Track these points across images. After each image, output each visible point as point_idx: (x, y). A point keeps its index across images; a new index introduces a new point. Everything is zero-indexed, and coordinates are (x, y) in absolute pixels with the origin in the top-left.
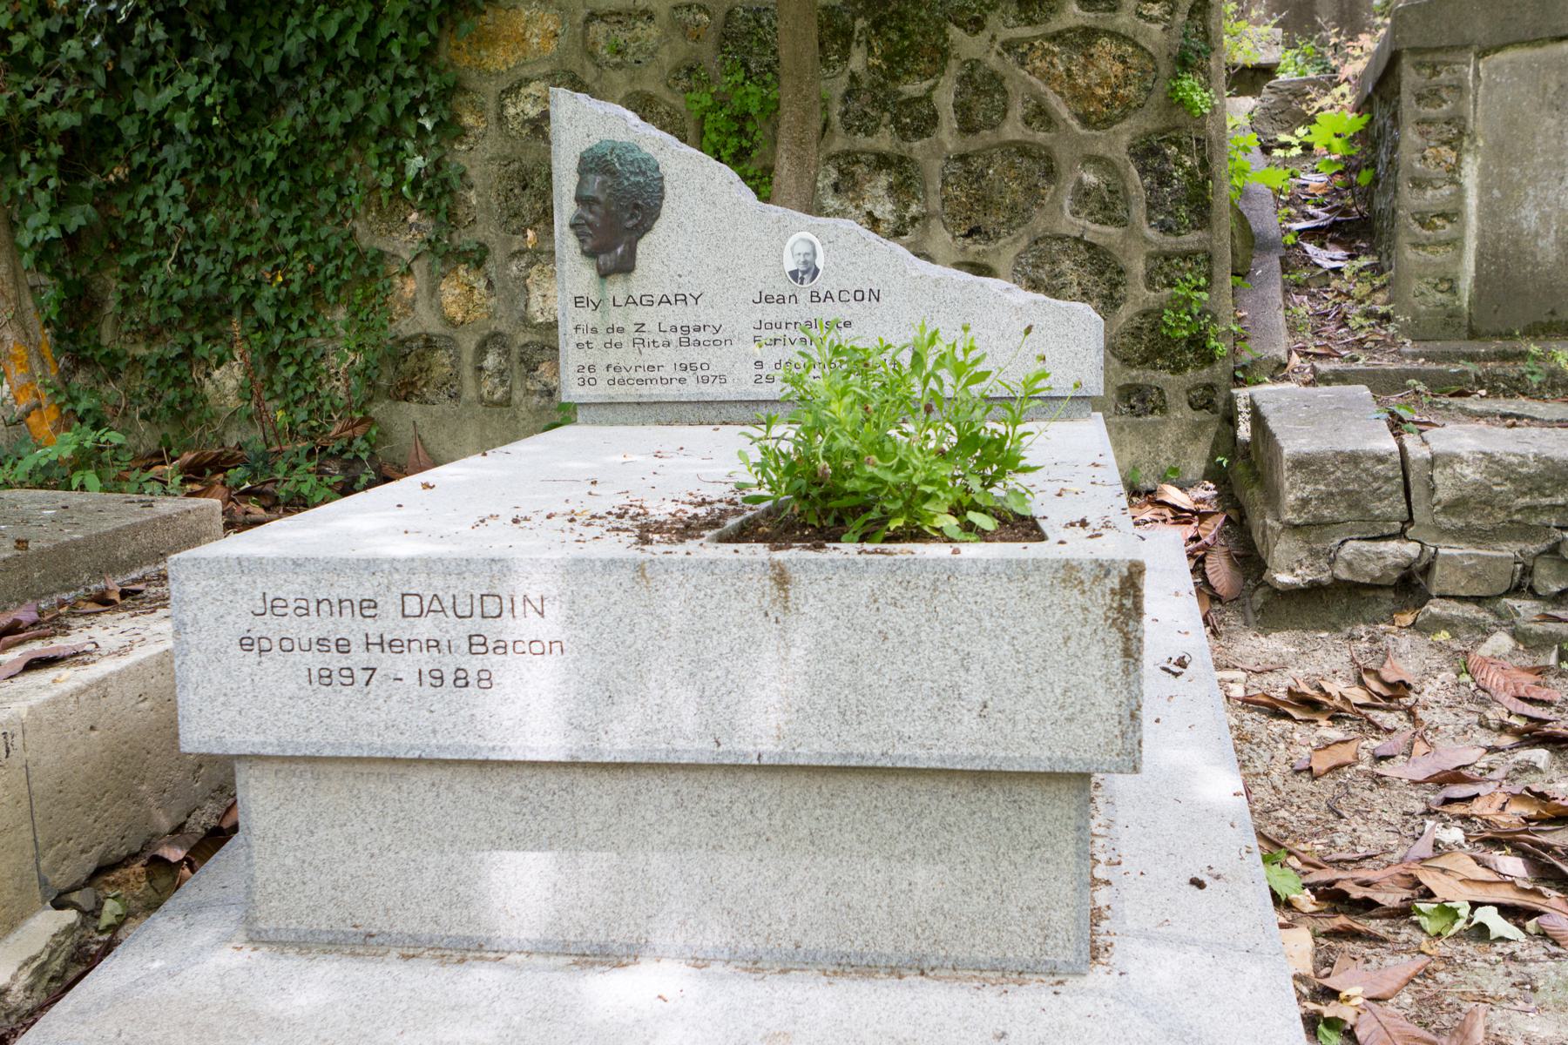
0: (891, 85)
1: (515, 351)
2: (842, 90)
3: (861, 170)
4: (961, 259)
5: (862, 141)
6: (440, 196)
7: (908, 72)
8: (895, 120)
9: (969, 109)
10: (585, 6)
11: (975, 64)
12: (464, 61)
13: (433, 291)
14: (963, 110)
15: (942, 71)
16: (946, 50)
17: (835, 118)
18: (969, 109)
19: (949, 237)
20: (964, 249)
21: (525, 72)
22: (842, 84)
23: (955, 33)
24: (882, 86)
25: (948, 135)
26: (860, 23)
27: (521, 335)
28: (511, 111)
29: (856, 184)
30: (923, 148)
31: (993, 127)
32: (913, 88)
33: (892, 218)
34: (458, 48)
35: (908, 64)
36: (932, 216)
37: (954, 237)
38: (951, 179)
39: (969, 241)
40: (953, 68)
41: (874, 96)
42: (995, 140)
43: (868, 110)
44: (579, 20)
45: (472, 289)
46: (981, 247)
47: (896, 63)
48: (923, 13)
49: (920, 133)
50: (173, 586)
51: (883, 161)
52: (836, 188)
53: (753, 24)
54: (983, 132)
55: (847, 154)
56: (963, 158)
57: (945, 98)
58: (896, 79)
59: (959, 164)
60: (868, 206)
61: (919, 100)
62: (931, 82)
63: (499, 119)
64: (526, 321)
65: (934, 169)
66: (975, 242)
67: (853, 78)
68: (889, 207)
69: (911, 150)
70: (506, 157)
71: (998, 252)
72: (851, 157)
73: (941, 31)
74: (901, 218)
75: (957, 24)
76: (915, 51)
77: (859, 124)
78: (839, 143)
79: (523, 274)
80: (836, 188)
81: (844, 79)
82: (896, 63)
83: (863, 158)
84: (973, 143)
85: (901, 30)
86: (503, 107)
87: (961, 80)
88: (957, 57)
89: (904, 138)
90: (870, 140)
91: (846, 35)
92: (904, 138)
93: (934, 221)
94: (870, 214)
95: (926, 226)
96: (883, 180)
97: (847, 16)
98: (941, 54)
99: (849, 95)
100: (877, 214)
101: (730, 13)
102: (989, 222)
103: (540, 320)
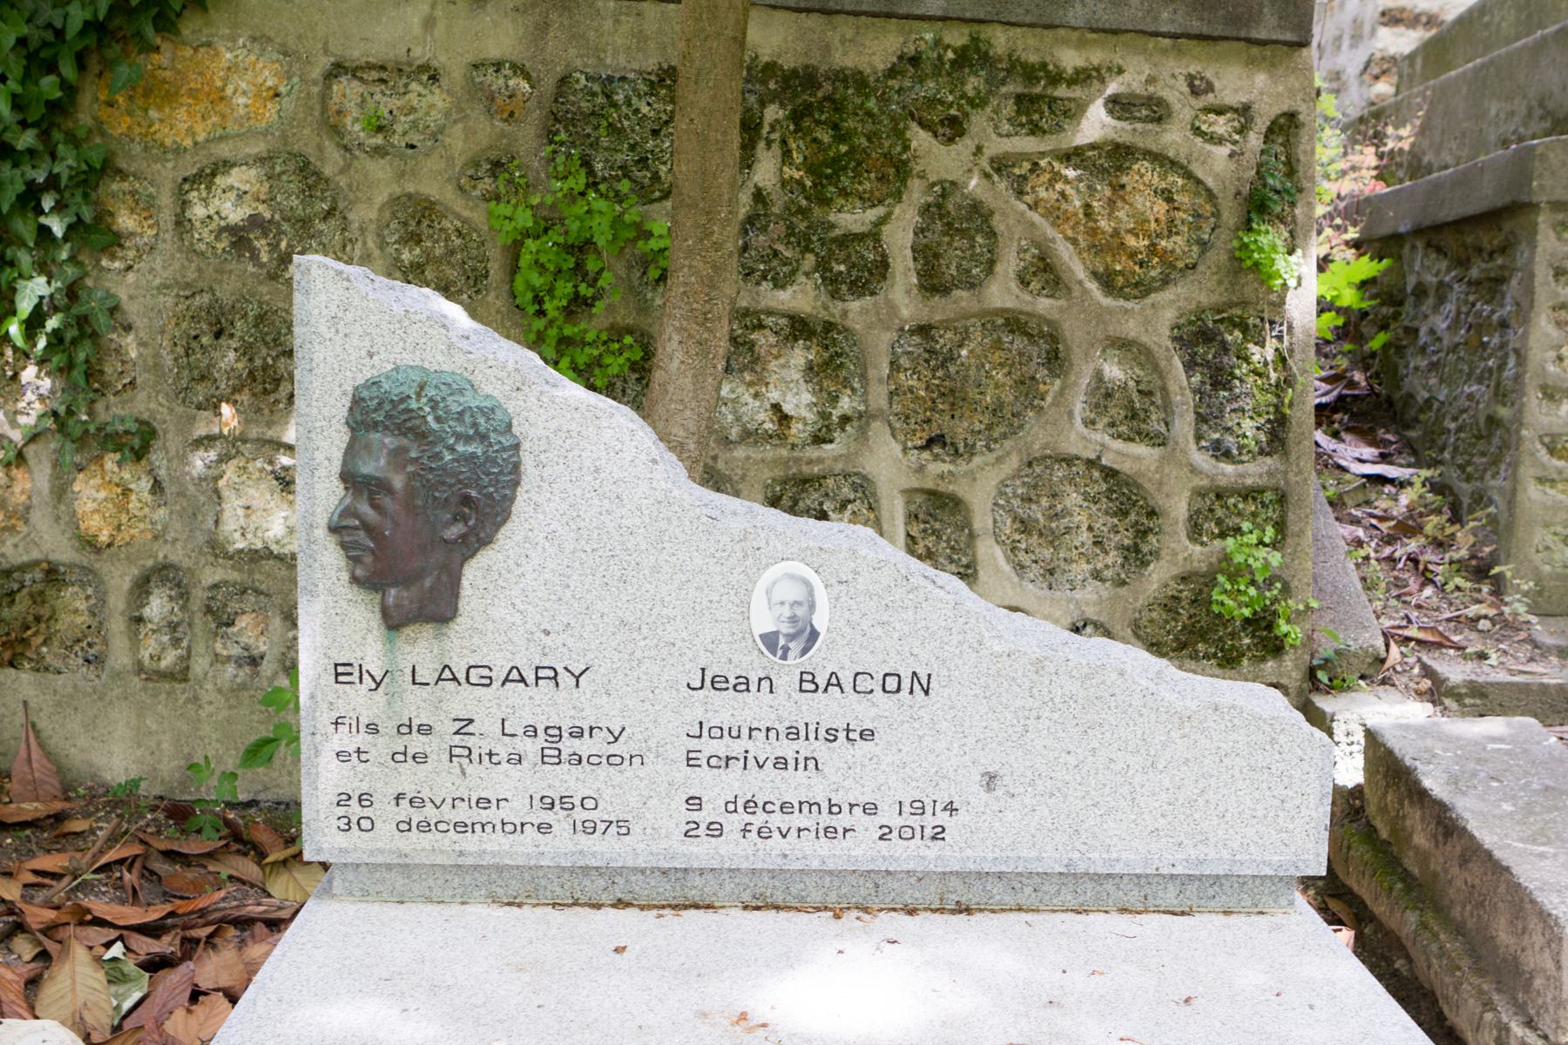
0: (817, 211)
4: (916, 484)
7: (844, 193)
9: (937, 256)
10: (326, 52)
11: (948, 188)
13: (61, 491)
15: (898, 196)
18: (937, 256)
20: (921, 469)
21: (224, 151)
23: (920, 138)
27: (208, 570)
28: (199, 211)
30: (864, 311)
31: (972, 286)
33: (811, 416)
35: (845, 181)
36: (874, 417)
37: (905, 450)
40: (917, 194)
42: (975, 307)
43: (780, 247)
44: (316, 73)
46: (946, 467)
48: (872, 104)
51: (799, 328)
54: (957, 293)
56: (924, 330)
59: (917, 339)
60: (774, 395)
61: (860, 237)
62: (880, 211)
63: (178, 223)
64: (216, 548)
65: (880, 344)
66: (936, 457)
68: (807, 397)
69: (845, 313)
70: (188, 285)
73: (899, 134)
75: (922, 124)
76: (856, 162)
83: (769, 321)
85: (835, 127)
86: (185, 204)
89: (835, 295)
92: (835, 295)
93: (876, 425)
94: (776, 407)
96: (799, 356)
98: (899, 170)
100: (788, 408)
101: (564, 80)
102: (960, 430)
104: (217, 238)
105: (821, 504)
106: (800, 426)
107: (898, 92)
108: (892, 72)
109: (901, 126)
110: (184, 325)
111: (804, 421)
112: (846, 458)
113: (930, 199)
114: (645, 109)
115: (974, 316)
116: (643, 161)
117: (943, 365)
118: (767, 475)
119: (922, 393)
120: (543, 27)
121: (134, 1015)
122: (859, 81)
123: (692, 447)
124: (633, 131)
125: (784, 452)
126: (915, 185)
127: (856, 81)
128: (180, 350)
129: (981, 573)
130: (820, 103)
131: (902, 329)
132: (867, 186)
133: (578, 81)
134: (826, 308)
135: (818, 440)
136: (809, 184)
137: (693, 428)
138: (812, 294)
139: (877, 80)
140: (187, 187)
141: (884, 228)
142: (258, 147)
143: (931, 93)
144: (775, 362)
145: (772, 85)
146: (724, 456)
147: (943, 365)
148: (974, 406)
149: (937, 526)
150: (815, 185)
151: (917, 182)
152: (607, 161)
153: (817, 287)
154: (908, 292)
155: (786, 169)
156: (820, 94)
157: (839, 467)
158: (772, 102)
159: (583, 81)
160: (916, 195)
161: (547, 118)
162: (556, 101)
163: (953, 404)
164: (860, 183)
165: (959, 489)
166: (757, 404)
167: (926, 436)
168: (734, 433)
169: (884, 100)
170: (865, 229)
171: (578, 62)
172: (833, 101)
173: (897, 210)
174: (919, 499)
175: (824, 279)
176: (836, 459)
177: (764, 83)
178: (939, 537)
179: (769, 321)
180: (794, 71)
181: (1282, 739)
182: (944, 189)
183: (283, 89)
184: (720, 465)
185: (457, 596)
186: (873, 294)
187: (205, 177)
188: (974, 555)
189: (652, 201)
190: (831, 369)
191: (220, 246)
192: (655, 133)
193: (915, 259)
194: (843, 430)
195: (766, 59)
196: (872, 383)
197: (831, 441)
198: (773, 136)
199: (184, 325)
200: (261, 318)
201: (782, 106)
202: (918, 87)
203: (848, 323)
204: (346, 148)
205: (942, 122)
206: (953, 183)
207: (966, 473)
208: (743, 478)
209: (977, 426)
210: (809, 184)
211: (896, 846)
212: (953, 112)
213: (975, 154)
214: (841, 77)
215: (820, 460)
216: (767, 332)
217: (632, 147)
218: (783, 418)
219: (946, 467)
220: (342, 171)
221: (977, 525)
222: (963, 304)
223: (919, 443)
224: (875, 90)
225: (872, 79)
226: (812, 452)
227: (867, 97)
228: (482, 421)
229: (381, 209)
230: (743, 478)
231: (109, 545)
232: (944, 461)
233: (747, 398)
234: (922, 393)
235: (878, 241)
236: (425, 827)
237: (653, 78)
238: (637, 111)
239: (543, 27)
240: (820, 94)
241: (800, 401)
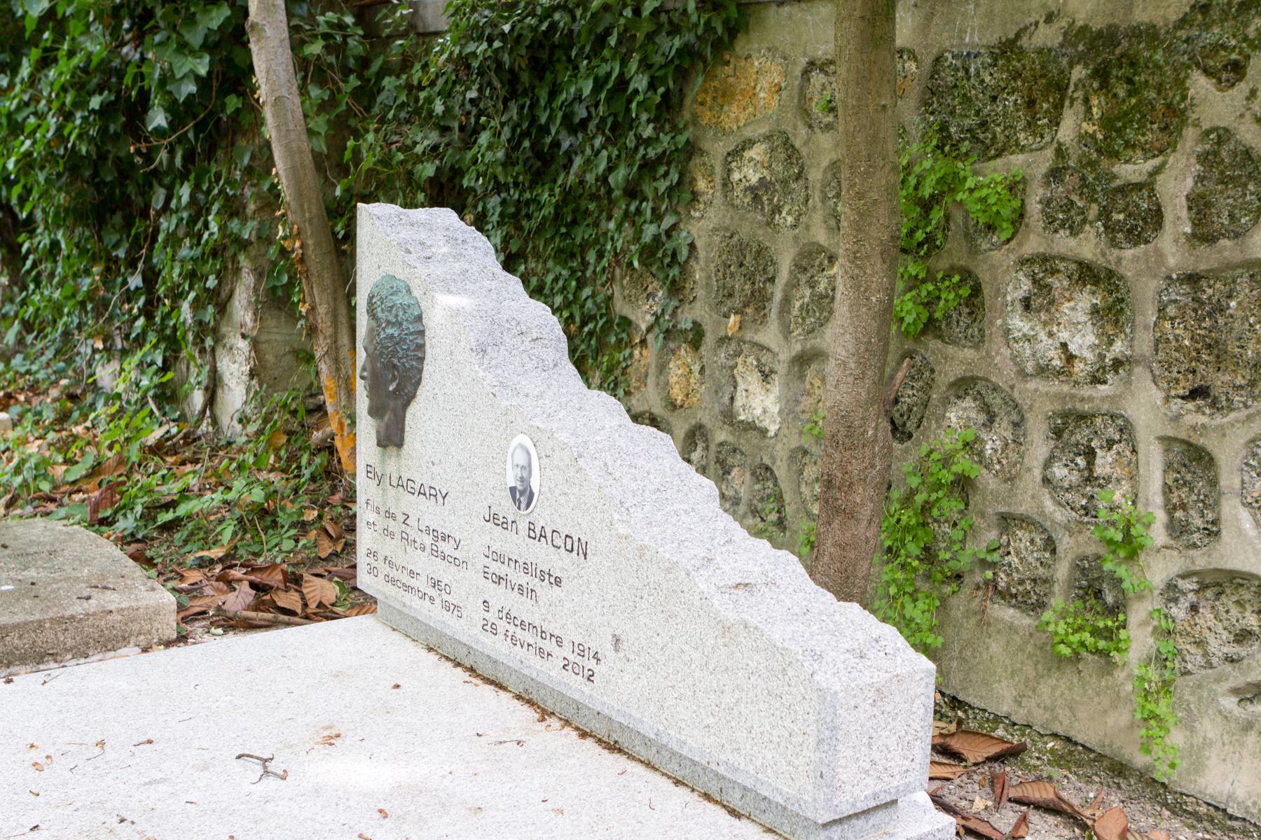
0: (1105, 163)
1: (713, 447)
2: (1044, 168)
3: (1058, 283)
4: (1170, 433)
5: (1064, 243)
6: (669, 266)
7: (1129, 145)
8: (1105, 214)
9: (1208, 205)
10: (805, 54)
11: (1223, 135)
12: (706, 117)
13: (662, 368)
14: (1199, 205)
15: (1172, 145)
16: (1183, 112)
17: (1034, 208)
18: (1208, 205)
19: (1157, 396)
20: (1177, 418)
21: (748, 133)
22: (1045, 160)
23: (1200, 84)
24: (1092, 164)
25: (1172, 246)
26: (1079, 72)
27: (718, 432)
28: (736, 176)
29: (1052, 302)
30: (1136, 259)
31: (1237, 235)
32: (1131, 170)
33: (1090, 356)
34: (702, 104)
35: (1130, 134)
36: (1137, 362)
37: (1167, 399)
38: (1171, 311)
39: (1190, 406)
40: (1190, 139)
41: (1083, 178)
42: (1237, 257)
43: (1075, 198)
44: (798, 71)
45: (691, 372)
46: (1202, 419)
47: (1115, 136)
48: (1159, 56)
49: (1135, 236)
50: (928, 761)
51: (1087, 274)
52: (1027, 304)
53: (961, 74)
54: (1224, 242)
55: (1045, 259)
56: (1193, 279)
57: (1177, 183)
58: (1115, 155)
59: (1186, 288)
60: (1064, 336)
61: (1138, 187)
62: (1156, 162)
63: (725, 185)
64: (728, 416)
65: (1146, 294)
66: (1199, 409)
67: (1060, 152)
68: (1091, 339)
69: (1119, 260)
70: (726, 229)
71: (1222, 431)
72: (1046, 261)
73: (1180, 84)
74: (1102, 357)
75: (1207, 72)
76: (1143, 114)
77: (1064, 218)
78: (1033, 244)
79: (731, 363)
80: (1027, 304)
81: (1049, 153)
82: (1115, 136)
83: (1061, 266)
84: (1206, 259)
85: (1130, 81)
86: (730, 171)
87: (1203, 158)
88: (1196, 124)
89: (1114, 243)
90: (1072, 242)
91: (1059, 88)
92: (1114, 243)
93: (1138, 370)
94: (1064, 345)
95: (1130, 373)
96: (1086, 299)
97: (1065, 61)
98: (1174, 118)
99: (1055, 174)
100: (1073, 348)
101: (938, 60)
102: (1219, 381)
103: (742, 418)
104: (745, 196)
105: (1090, 440)
106: (1082, 365)
107: (1187, 41)
108: (1183, 22)
109: (1182, 75)
110: (724, 257)
111: (1084, 360)
112: (1112, 399)
113: (1207, 147)
114: (987, 79)
115: (1238, 266)
116: (983, 124)
117: (1210, 315)
118: (1049, 408)
119: (1187, 342)
120: (929, 17)
121: (694, 738)
122: (1150, 34)
123: (853, 365)
124: (977, 99)
125: (1066, 388)
126: (1190, 134)
127: (1148, 35)
128: (720, 274)
129: (1224, 533)
130: (1118, 59)
131: (1169, 277)
132: (1149, 136)
133: (946, 60)
134: (1104, 255)
135: (1096, 380)
136: (1100, 136)
137: (852, 350)
138: (1094, 241)
139: (1167, 32)
140: (730, 159)
141: (1158, 178)
142: (763, 129)
143: (1214, 40)
144: (1067, 305)
145: (1081, 48)
146: (1019, 386)
147: (1210, 315)
148: (1237, 362)
149: (1189, 477)
150: (1105, 138)
151: (1191, 130)
152: (959, 125)
153: (1098, 235)
154: (1176, 241)
155: (1084, 125)
156: (1118, 51)
157: (1105, 407)
158: (1078, 63)
159: (950, 59)
160: (1189, 144)
161: (923, 93)
162: (932, 77)
163: (1218, 357)
164: (1144, 135)
165: (1209, 443)
166: (1050, 341)
167: (1189, 386)
168: (1030, 367)
169: (1170, 50)
170: (1142, 179)
171: (947, 43)
172: (1128, 57)
173: (1171, 160)
174: (1177, 448)
175: (1106, 227)
176: (1103, 399)
177: (1075, 46)
178: (1192, 490)
179: (1061, 266)
180: (1100, 32)
181: (790, 673)
182: (1219, 136)
183: (783, 85)
184: (1016, 395)
185: (403, 430)
186: (1147, 242)
187: (737, 153)
188: (1219, 513)
189: (990, 159)
190: (1113, 314)
191: (746, 201)
192: (994, 99)
193: (1190, 208)
194: (1117, 372)
195: (1080, 23)
196: (1138, 329)
197: (1105, 382)
198: (1075, 95)
199: (724, 257)
200: (759, 253)
201: (1086, 66)
202: (1204, 34)
203: (1122, 270)
204: (810, 127)
205: (1225, 67)
206: (1226, 130)
207: (1217, 427)
208: (1031, 408)
209: (1240, 381)
210: (1100, 136)
211: (568, 677)
212: (1234, 56)
213: (1248, 99)
214: (1136, 33)
215: (1091, 399)
216: (1061, 276)
217: (978, 113)
218: (1070, 358)
219: (1202, 419)
220: (805, 143)
221: (1223, 483)
222: (1226, 254)
223: (1181, 392)
224: (1162, 42)
225: (1162, 31)
226: (1087, 391)
227: (1155, 49)
228: (401, 313)
229: (824, 172)
230: (1031, 408)
231: (682, 406)
232: (1204, 414)
233: (1042, 336)
234: (1187, 342)
235: (1153, 190)
236: (393, 582)
237: (997, 51)
238: (983, 81)
239: (929, 17)
240: (1118, 51)
241: (1083, 341)
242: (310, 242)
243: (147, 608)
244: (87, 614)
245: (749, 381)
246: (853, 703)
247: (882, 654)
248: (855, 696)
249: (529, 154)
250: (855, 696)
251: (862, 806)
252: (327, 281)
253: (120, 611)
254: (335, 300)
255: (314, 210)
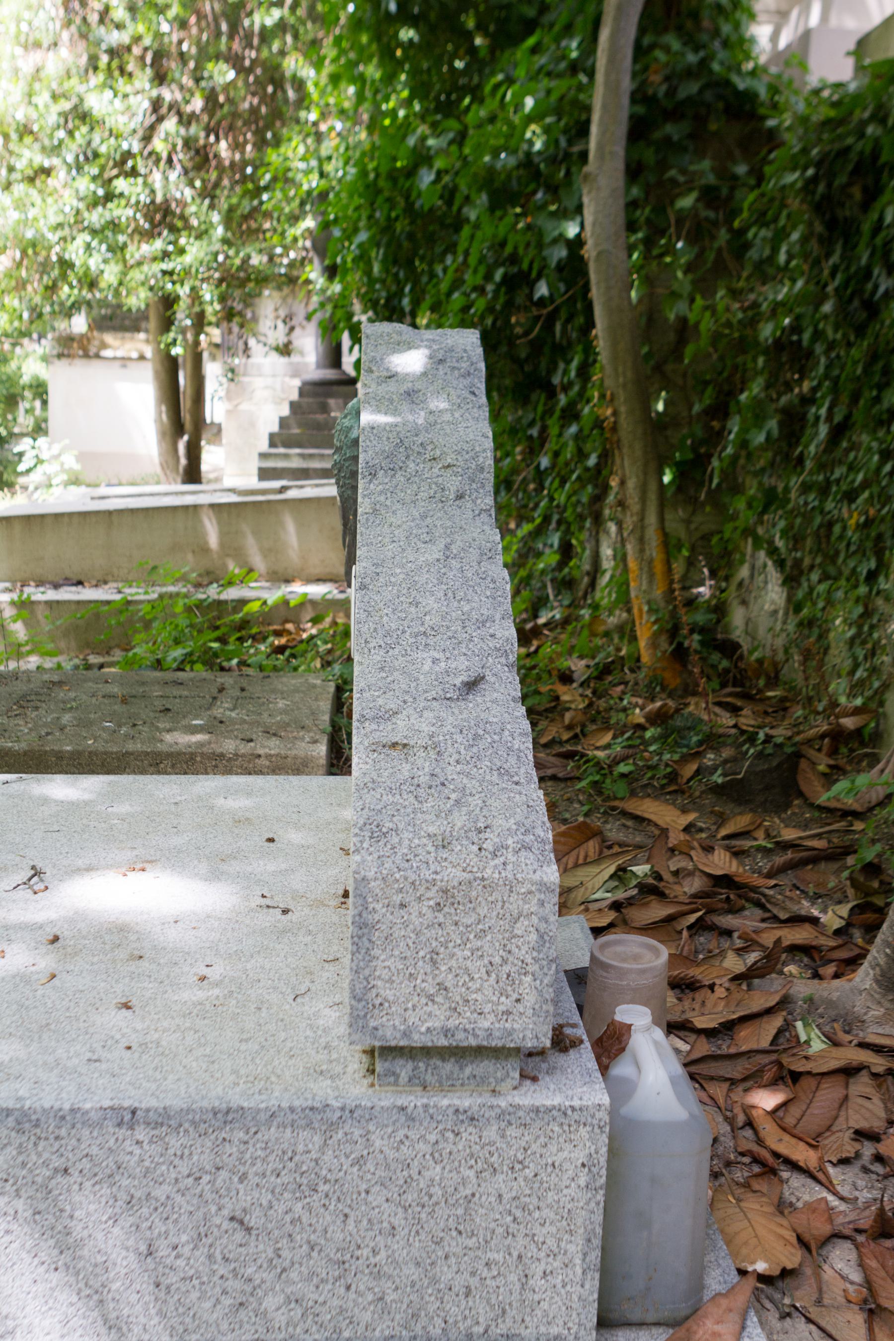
242: (623, 409)
243: (295, 758)
244: (236, 755)
245: (542, 467)
246: (397, 899)
247: (475, 848)
248: (401, 890)
249: (797, 248)
250: (401, 890)
251: (418, 1040)
252: (639, 453)
253: (268, 756)
254: (645, 474)
255: (629, 374)
